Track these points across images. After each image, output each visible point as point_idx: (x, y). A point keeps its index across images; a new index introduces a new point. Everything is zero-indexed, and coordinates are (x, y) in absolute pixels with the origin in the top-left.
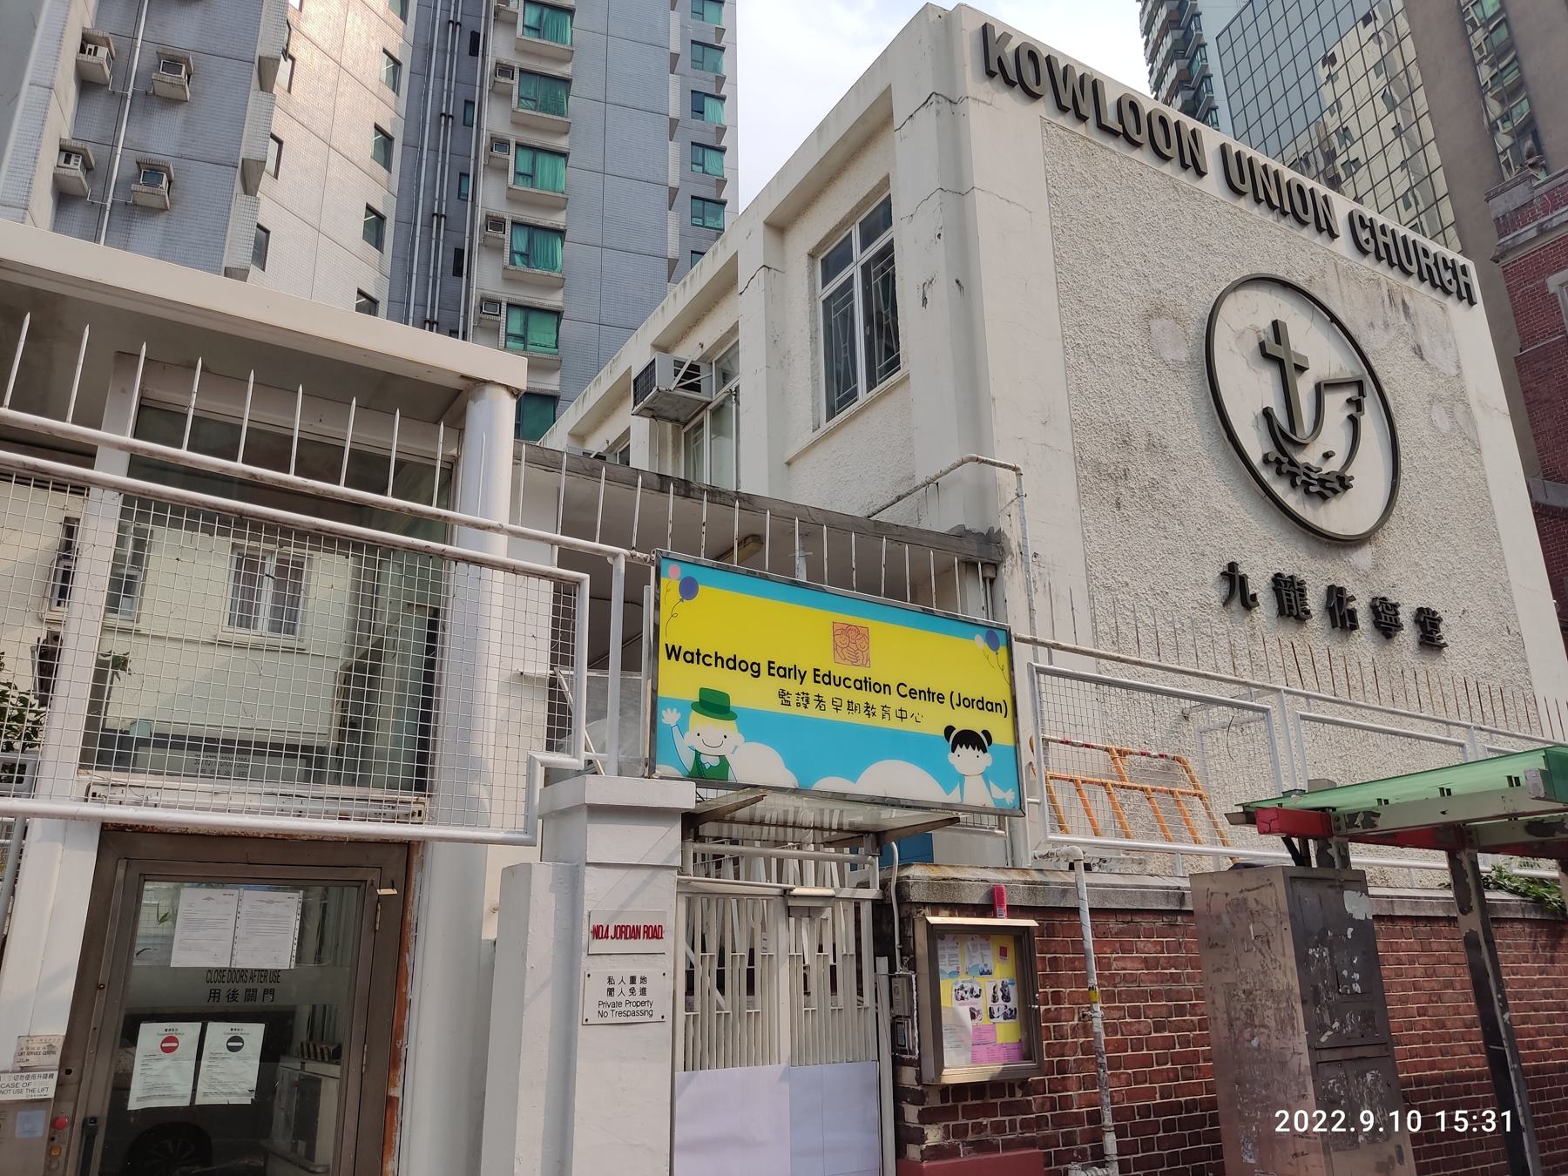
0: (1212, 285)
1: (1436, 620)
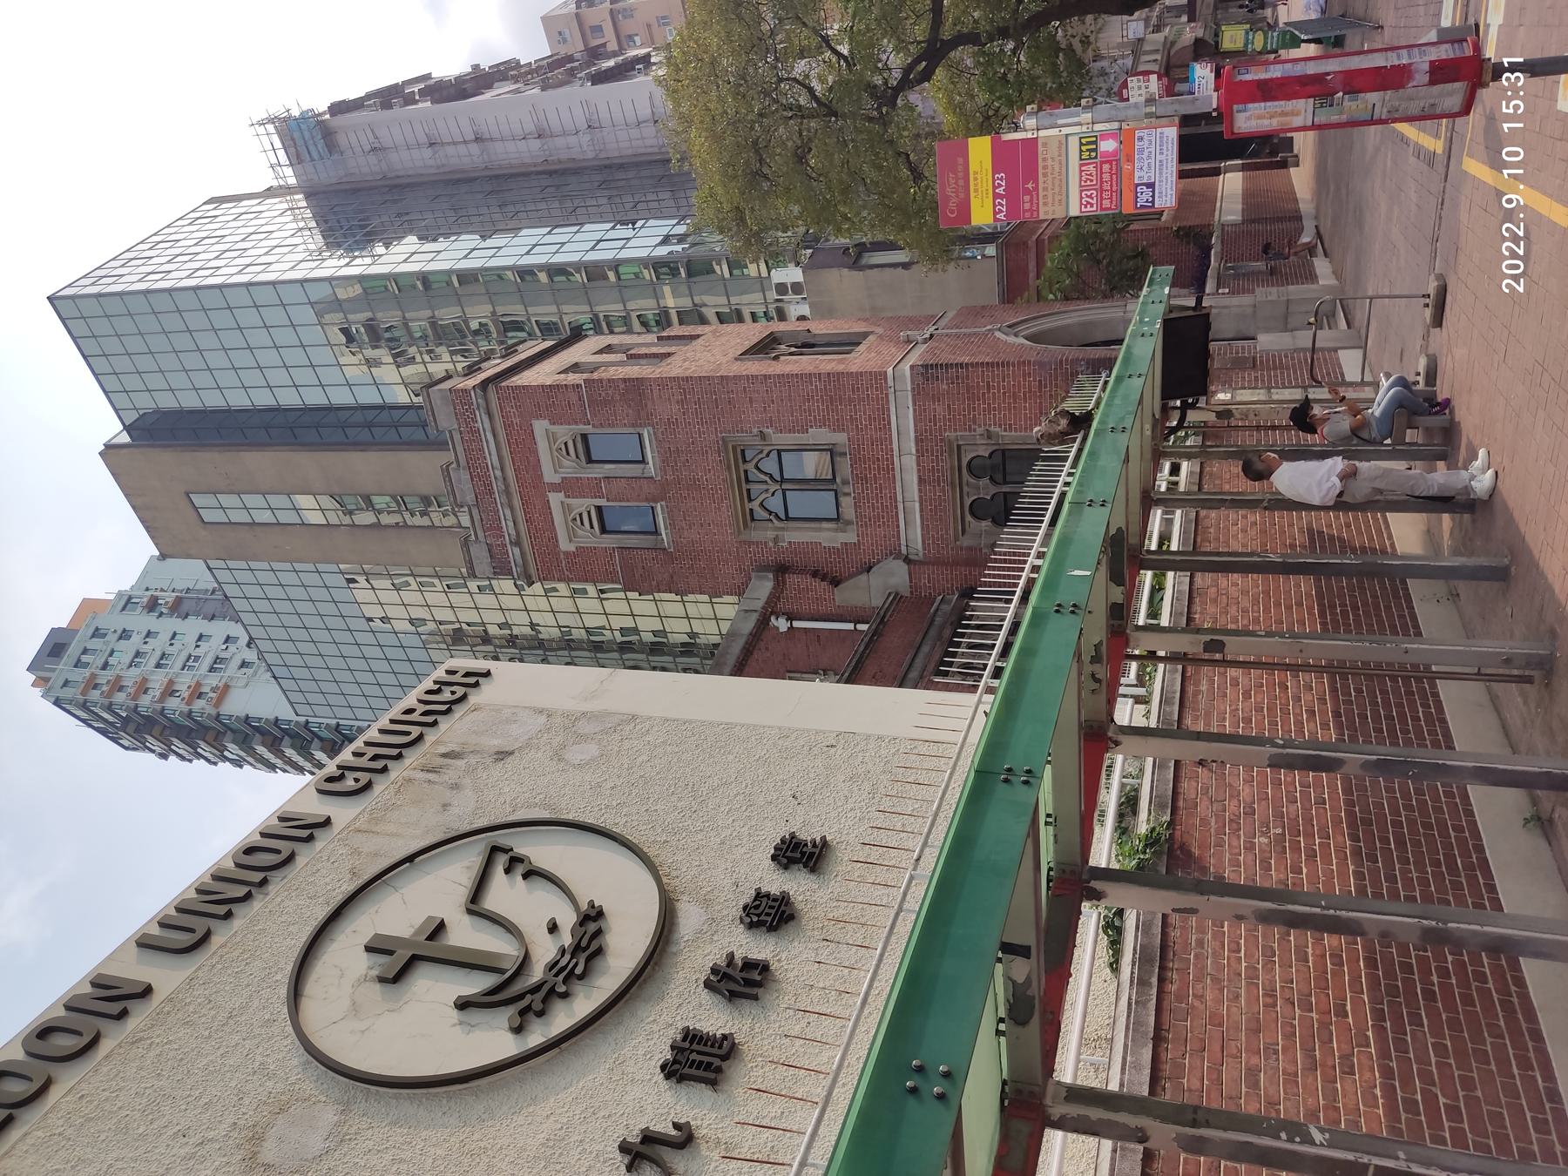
0: (276, 1029)
1: (791, 841)
